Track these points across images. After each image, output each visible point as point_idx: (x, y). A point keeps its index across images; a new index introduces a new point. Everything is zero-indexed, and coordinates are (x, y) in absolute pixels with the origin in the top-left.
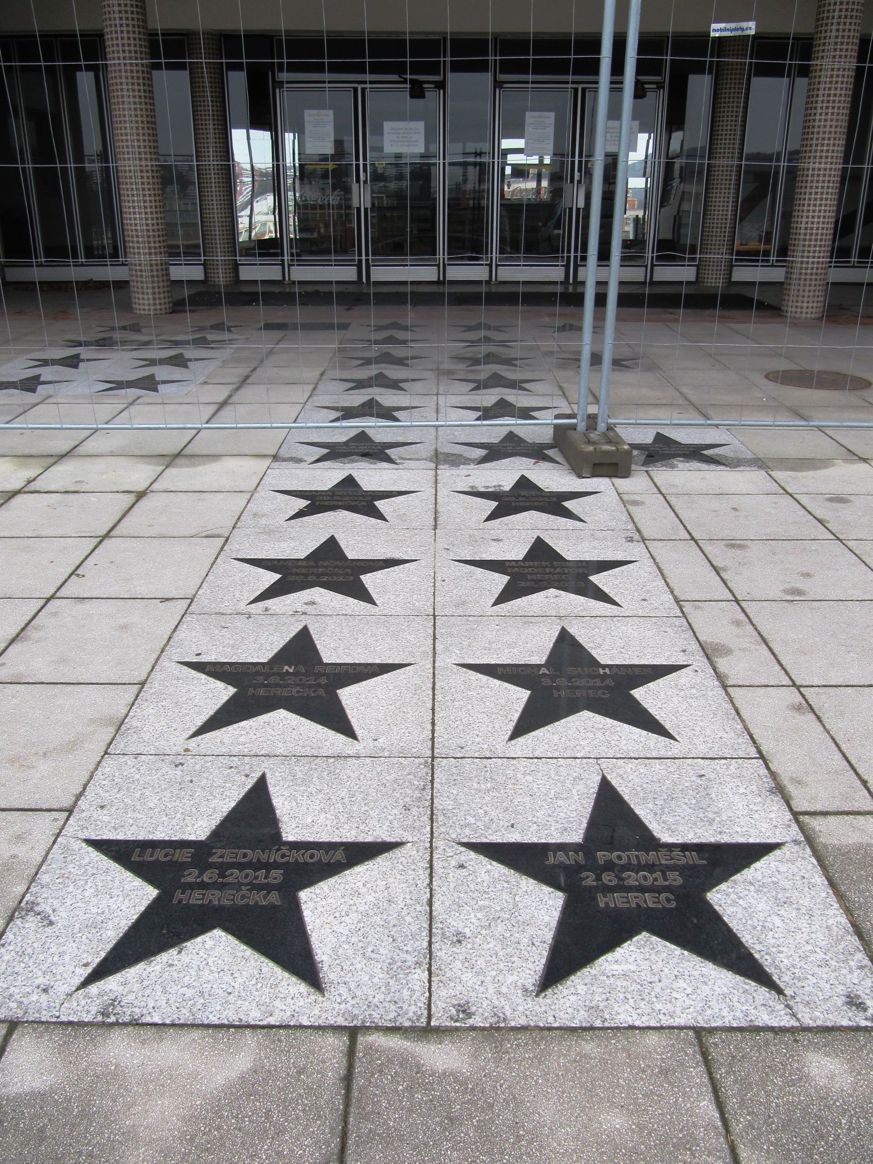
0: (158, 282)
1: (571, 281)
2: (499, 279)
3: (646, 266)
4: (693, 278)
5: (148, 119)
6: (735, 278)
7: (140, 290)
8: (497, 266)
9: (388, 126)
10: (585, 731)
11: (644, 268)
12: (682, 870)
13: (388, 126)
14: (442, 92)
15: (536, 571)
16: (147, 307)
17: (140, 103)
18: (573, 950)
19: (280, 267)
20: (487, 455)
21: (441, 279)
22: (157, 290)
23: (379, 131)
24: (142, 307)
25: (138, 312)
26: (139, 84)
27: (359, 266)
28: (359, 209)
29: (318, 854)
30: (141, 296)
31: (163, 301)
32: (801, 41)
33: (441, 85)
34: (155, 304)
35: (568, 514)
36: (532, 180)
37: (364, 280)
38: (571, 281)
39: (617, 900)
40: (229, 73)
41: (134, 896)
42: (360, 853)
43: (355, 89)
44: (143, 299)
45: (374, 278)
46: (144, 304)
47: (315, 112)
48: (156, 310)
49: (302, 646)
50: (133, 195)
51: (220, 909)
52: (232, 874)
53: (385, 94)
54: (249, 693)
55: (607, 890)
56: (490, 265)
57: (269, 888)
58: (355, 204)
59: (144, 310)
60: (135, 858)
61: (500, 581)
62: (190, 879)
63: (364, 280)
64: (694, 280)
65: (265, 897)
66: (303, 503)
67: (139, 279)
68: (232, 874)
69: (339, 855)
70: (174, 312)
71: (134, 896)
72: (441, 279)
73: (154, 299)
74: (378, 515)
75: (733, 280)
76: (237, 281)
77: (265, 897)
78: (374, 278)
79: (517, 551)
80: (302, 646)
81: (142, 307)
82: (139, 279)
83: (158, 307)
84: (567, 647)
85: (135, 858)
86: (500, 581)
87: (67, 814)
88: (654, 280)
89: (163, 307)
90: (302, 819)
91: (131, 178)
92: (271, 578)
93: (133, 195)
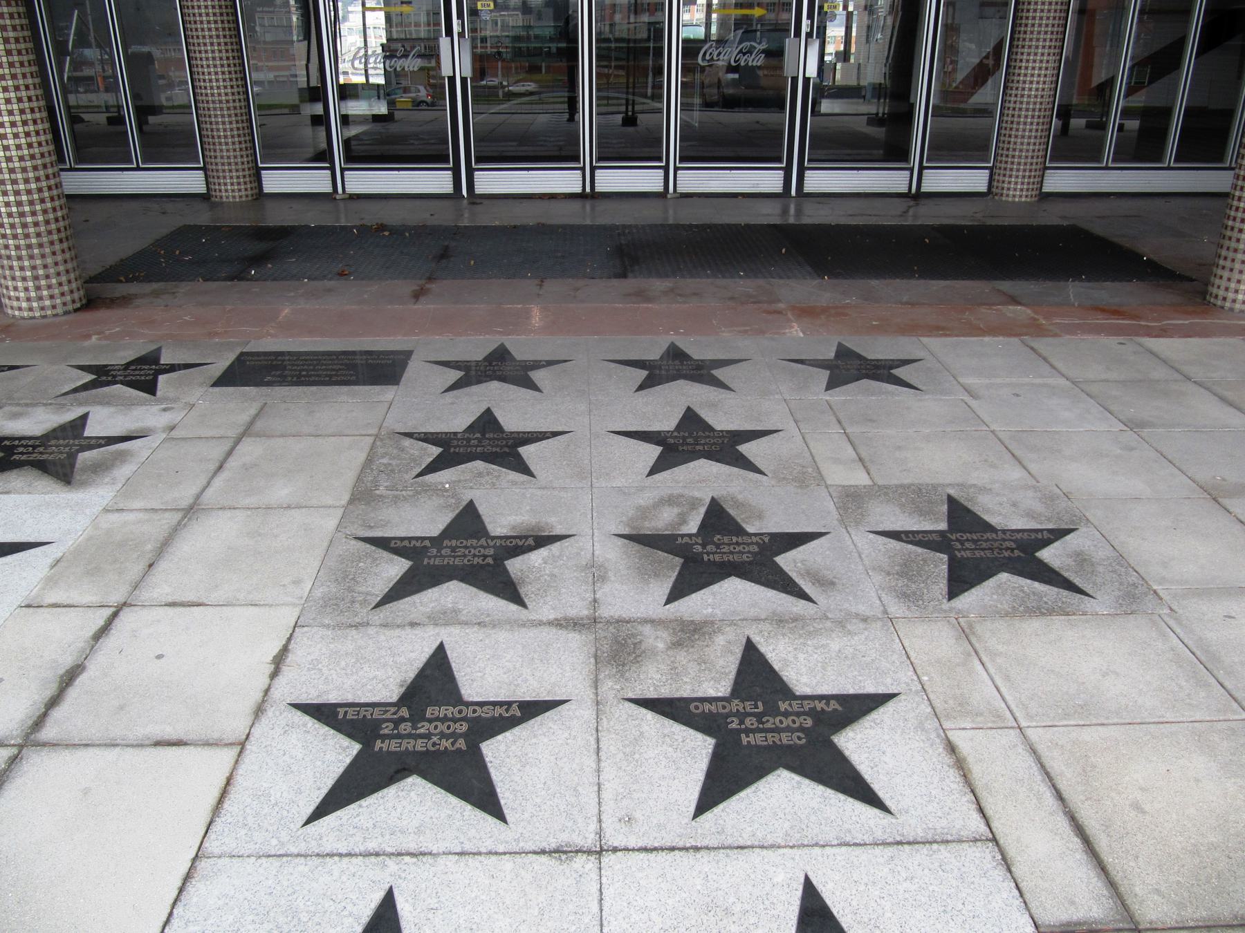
1: (793, 192)
2: (679, 190)
3: (912, 170)
4: (983, 188)
6: (1047, 188)
8: (676, 169)
10: (733, 598)
11: (907, 173)
12: (812, 713)
15: (685, 442)
16: (24, 305)
18: (720, 785)
19: (328, 172)
20: (648, 377)
21: (588, 189)
24: (15, 304)
25: (10, 311)
27: (456, 171)
29: (499, 711)
32: (135, 166)
34: (40, 298)
35: (746, 464)
36: (839, 26)
37: (464, 192)
38: (793, 192)
39: (757, 739)
41: (338, 753)
42: (532, 709)
44: (16, 289)
45: (479, 189)
46: (18, 299)
48: (42, 308)
51: (455, 567)
54: (377, 749)
55: (748, 731)
57: (454, 736)
59: (20, 309)
60: (392, 545)
61: (654, 451)
62: (386, 731)
63: (464, 192)
64: (984, 189)
65: (453, 744)
66: (455, 375)
69: (531, 542)
70: (90, 303)
71: (338, 753)
72: (588, 189)
73: (38, 288)
74: (532, 386)
75: (1045, 190)
76: (260, 195)
77: (453, 744)
78: (479, 189)
79: (667, 423)
80: (468, 521)
81: (15, 304)
84: (690, 419)
85: (392, 545)
86: (654, 451)
87: (239, 748)
88: (923, 190)
90: (483, 676)
92: (455, 375)
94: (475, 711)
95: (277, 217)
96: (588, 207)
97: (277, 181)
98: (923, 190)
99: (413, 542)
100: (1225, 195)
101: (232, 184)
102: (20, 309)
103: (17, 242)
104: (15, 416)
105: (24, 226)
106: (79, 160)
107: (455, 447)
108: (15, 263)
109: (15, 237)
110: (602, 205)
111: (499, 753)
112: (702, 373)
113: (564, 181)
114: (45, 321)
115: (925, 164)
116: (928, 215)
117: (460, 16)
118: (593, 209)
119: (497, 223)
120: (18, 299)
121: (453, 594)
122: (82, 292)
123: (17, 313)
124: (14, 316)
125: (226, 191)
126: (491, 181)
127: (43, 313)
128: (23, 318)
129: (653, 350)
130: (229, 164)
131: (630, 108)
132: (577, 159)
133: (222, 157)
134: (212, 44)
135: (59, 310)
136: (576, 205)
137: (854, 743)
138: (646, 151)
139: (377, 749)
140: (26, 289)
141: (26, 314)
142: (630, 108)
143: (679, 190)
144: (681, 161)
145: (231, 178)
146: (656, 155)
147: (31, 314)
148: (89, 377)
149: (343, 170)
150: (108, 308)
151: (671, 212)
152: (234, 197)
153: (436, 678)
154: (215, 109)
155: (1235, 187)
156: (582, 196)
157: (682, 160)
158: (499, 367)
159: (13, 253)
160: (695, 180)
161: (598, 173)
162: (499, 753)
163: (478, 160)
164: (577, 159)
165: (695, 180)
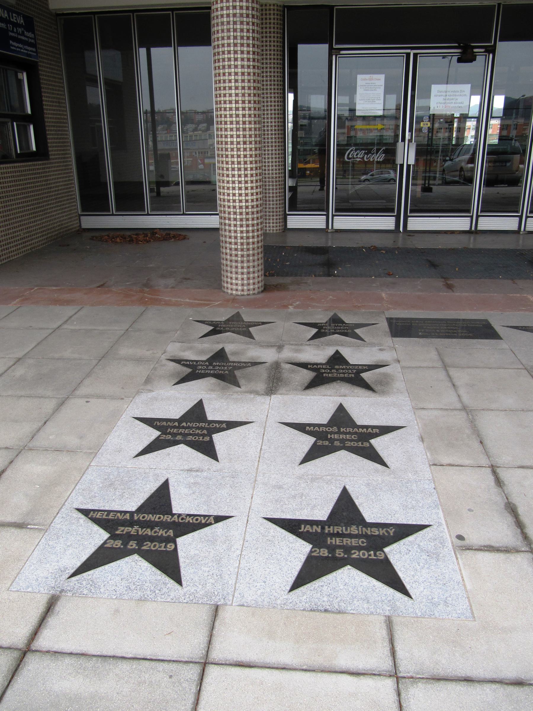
0: (254, 261)
5: (256, 85)
7: (234, 270)
8: (527, 217)
9: (435, 88)
11: (517, 219)
13: (435, 88)
14: (491, 56)
16: (240, 288)
17: (249, 67)
21: (473, 229)
22: (251, 270)
23: (428, 95)
24: (234, 287)
26: (248, 45)
28: (402, 166)
30: (234, 276)
31: (256, 281)
33: (492, 50)
40: (179, 48)
43: (408, 55)
45: (410, 227)
47: (367, 76)
48: (249, 290)
49: (197, 412)
50: (233, 169)
52: (147, 544)
53: (433, 62)
56: (521, 217)
58: (399, 161)
59: (237, 290)
67: (234, 258)
68: (147, 544)
69: (224, 425)
72: (473, 229)
76: (285, 229)
78: (410, 227)
80: (197, 412)
81: (234, 287)
82: (234, 258)
83: (251, 287)
89: (256, 286)
91: (232, 150)
93: (233, 169)
94: (197, 520)
95: (293, 241)
96: (472, 238)
97: (295, 221)
98: (479, 228)
99: (169, 423)
100: (217, 230)
101: (273, 223)
102: (237, 290)
103: (242, 253)
104: (297, 351)
105: (248, 244)
106: (118, 210)
107: (199, 370)
108: (239, 265)
109: (242, 250)
110: (480, 238)
111: (187, 546)
112: (348, 331)
113: (460, 223)
114: (249, 297)
115: (528, 215)
116: (483, 243)
117: (411, 130)
118: (475, 239)
119: (440, 247)
120: (237, 284)
121: (182, 451)
122: (263, 283)
123: (234, 292)
124: (232, 294)
125: (269, 227)
126: (416, 223)
127: (248, 293)
128: (237, 295)
129: (322, 318)
130: (273, 212)
131: (427, 182)
132: (468, 211)
133: (269, 208)
134: (272, 146)
135: (256, 291)
136: (465, 237)
137: (397, 554)
138: (460, 207)
139: (329, 543)
140: (243, 279)
141: (239, 293)
142: (427, 182)
143: (527, 229)
144: (335, 212)
145: (273, 219)
146: (516, 210)
147: (242, 293)
148: (357, 331)
149: (333, 216)
150: (278, 290)
151: (521, 242)
152: (273, 230)
153: (161, 499)
154: (269, 182)
155: (221, 224)
156: (469, 232)
157: (337, 210)
158: (336, 326)
159: (239, 259)
160: (343, 222)
161: (480, 219)
162: (187, 546)
163: (411, 211)
164: (468, 211)
165: (343, 222)
